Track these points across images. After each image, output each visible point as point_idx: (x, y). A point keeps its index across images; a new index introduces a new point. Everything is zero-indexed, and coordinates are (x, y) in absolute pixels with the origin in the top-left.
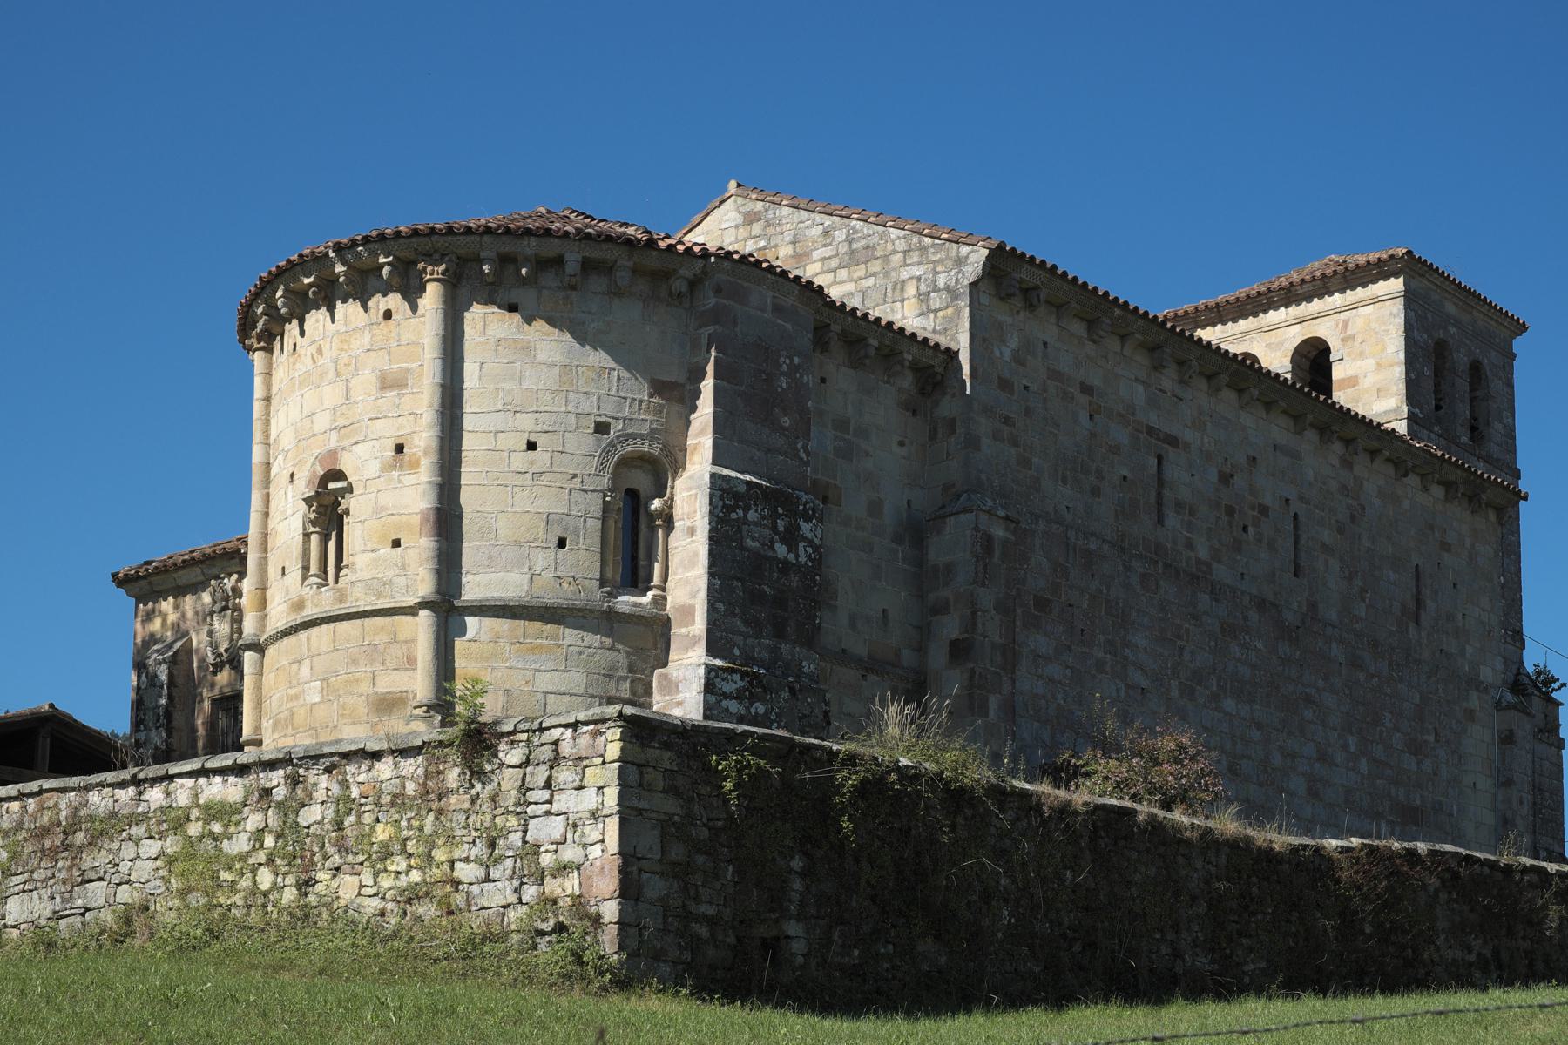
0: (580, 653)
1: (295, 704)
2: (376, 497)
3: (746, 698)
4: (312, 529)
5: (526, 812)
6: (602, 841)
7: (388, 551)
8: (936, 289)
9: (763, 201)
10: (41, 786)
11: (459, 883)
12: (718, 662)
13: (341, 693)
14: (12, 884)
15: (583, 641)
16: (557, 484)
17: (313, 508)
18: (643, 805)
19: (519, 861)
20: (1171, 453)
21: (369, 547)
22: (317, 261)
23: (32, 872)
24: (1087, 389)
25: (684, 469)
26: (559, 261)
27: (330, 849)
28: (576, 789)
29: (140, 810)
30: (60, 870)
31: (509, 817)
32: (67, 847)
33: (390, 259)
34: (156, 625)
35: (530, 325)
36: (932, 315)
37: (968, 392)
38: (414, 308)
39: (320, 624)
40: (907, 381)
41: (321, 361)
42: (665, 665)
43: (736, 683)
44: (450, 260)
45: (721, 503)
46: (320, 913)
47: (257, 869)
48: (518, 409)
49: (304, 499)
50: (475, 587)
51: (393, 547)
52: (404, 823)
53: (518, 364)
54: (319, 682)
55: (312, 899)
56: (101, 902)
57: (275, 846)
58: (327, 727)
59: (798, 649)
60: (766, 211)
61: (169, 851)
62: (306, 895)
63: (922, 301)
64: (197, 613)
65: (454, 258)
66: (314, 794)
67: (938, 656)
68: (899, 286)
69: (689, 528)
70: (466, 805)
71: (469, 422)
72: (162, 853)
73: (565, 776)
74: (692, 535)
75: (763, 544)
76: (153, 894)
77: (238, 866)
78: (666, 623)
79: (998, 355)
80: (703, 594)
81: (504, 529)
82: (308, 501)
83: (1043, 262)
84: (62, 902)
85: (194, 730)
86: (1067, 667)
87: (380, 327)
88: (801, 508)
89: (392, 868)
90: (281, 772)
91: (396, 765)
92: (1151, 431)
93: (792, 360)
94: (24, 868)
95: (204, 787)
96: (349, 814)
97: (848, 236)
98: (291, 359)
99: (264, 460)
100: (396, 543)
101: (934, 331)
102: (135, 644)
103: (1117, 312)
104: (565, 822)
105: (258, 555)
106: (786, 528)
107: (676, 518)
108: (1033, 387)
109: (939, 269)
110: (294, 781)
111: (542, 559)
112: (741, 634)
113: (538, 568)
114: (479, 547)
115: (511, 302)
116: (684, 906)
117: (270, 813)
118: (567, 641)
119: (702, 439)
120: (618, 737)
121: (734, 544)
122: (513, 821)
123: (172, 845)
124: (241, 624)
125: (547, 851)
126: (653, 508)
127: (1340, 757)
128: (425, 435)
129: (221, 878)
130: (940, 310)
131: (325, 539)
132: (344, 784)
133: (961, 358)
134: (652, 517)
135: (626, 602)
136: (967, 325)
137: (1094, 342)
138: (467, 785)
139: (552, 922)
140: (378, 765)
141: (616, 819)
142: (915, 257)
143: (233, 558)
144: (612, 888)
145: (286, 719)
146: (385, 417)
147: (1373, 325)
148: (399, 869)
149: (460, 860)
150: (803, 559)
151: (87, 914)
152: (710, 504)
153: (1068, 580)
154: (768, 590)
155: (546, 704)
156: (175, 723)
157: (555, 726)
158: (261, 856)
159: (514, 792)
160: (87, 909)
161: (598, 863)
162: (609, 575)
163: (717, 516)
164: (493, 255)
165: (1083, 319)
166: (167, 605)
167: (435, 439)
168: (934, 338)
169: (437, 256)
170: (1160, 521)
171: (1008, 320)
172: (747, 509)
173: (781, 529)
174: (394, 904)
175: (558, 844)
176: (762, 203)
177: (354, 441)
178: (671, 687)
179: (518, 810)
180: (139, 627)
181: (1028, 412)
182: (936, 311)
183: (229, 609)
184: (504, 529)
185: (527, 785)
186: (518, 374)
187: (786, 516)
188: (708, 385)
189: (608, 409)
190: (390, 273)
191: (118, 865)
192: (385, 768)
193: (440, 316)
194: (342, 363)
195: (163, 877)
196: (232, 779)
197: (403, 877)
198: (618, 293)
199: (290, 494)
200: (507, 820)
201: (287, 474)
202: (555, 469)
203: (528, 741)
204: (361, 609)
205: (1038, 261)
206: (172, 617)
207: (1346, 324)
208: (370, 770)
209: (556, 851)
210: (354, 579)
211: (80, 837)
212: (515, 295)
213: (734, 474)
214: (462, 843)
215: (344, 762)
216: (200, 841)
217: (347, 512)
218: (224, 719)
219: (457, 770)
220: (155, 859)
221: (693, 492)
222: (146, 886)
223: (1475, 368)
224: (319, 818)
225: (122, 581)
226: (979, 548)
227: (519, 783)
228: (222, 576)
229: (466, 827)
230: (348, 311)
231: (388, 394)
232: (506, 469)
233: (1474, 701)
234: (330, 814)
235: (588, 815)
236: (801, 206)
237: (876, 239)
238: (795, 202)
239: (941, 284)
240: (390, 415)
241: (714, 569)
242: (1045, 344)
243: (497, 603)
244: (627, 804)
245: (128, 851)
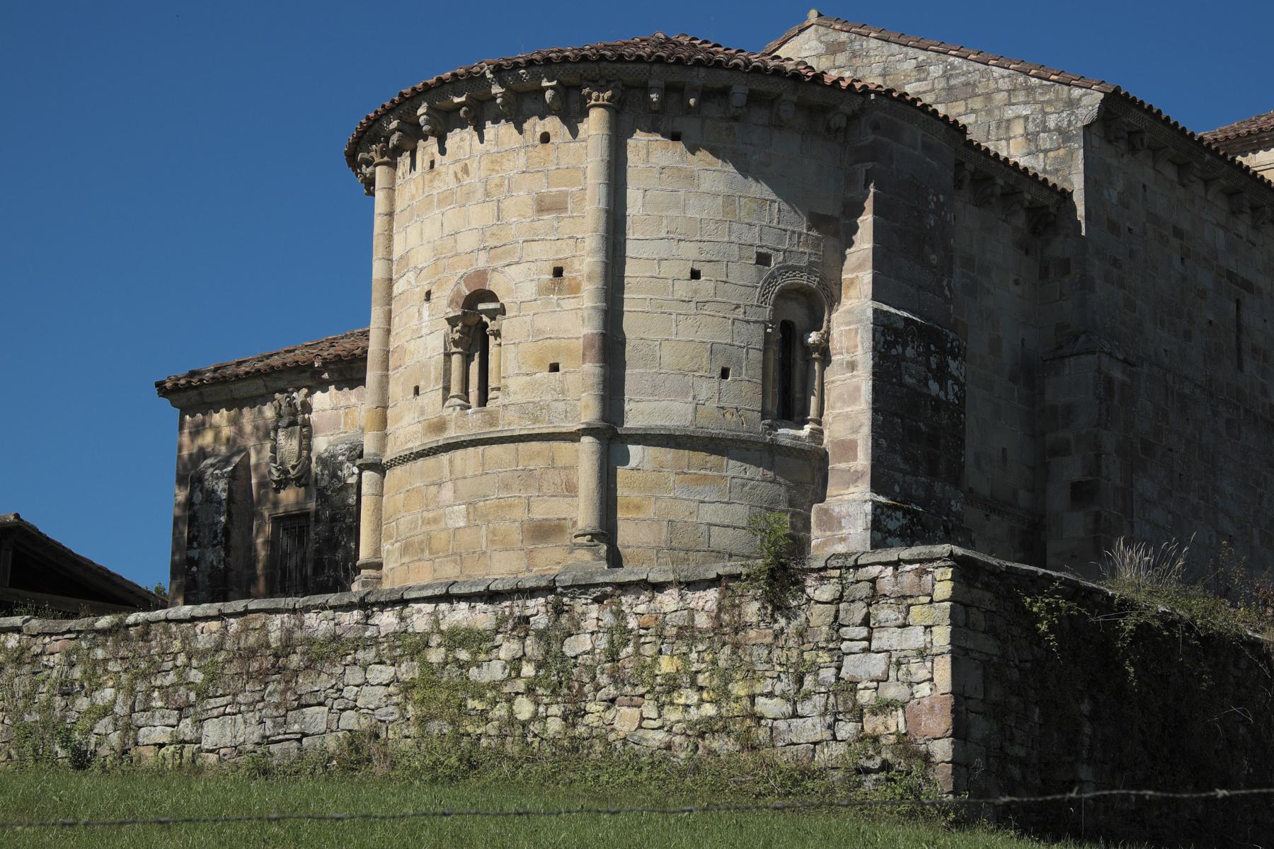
0: (743, 485)
1: (434, 527)
2: (532, 321)
3: (908, 536)
4: (454, 349)
5: (840, 649)
6: (931, 680)
7: (545, 374)
8: (1045, 129)
9: (848, 32)
10: (246, 606)
11: (762, 718)
12: (882, 499)
13: (491, 517)
14: (209, 707)
15: (746, 472)
16: (720, 314)
17: (458, 328)
18: (970, 645)
19: (832, 697)
21: (524, 370)
22: (473, 81)
23: (235, 695)
24: (1178, 233)
25: (839, 303)
26: (725, 93)
27: (603, 679)
28: (899, 627)
29: (368, 634)
30: (270, 694)
31: (821, 653)
32: (280, 670)
33: (554, 83)
34: (207, 439)
35: (694, 154)
36: (1041, 156)
37: (1083, 233)
38: (574, 133)
39: (466, 447)
40: (1021, 221)
41: (467, 181)
42: (822, 500)
43: (898, 520)
44: (616, 87)
45: (882, 339)
46: (591, 746)
47: (514, 698)
48: (682, 238)
49: (447, 319)
50: (637, 415)
51: (551, 371)
52: (694, 656)
53: (682, 193)
54: (464, 506)
55: (581, 730)
56: (323, 727)
57: (536, 676)
58: (474, 553)
59: (947, 487)
60: (851, 41)
61: (406, 677)
62: (574, 725)
63: (1030, 141)
64: (257, 428)
65: (620, 85)
66: (583, 624)
67: (532, 574)
68: (1004, 124)
69: (848, 363)
70: (769, 640)
71: (631, 249)
72: (395, 680)
73: (885, 613)
74: (853, 370)
75: (919, 381)
76: (384, 721)
77: (489, 695)
78: (824, 457)
79: (1107, 197)
80: (866, 430)
81: (668, 357)
82: (452, 321)
83: (1150, 107)
84: (274, 726)
85: (251, 548)
86: (1169, 512)
87: (536, 150)
88: (949, 345)
89: (682, 701)
90: (541, 600)
91: (682, 597)
92: (1231, 276)
93: (938, 199)
94: (225, 690)
95: (446, 613)
96: (626, 645)
97: (945, 72)
98: (428, 177)
99: (386, 276)
101: (1045, 171)
102: (179, 457)
103: (1208, 157)
105: (379, 372)
106: (938, 367)
107: (832, 352)
110: (558, 610)
111: (706, 389)
112: (901, 471)
113: (702, 397)
114: (642, 375)
115: (676, 130)
116: (1001, 748)
117: (528, 642)
118: (730, 473)
119: (861, 274)
120: (949, 576)
121: (894, 380)
122: (824, 658)
123: (408, 671)
124: (310, 440)
125: (866, 688)
126: (810, 340)
128: (589, 260)
129: (469, 706)
130: (1050, 150)
131: (467, 360)
132: (619, 614)
133: (1075, 199)
134: (808, 349)
135: (785, 434)
136: (1081, 167)
137: (1184, 186)
138: (768, 620)
139: (878, 760)
140: (660, 597)
141: (948, 658)
142: (1021, 96)
143: (304, 372)
144: (944, 727)
145: (421, 543)
146: (543, 240)
148: (689, 702)
149: (762, 695)
150: (951, 397)
151: (304, 740)
152: (873, 340)
153: (1168, 424)
155: (710, 536)
156: (233, 542)
157: (873, 564)
158: (520, 685)
159: (825, 629)
160: (305, 735)
161: (926, 702)
162: (769, 407)
163: (879, 352)
164: (662, 84)
165: (1174, 163)
166: (220, 418)
167: (600, 264)
168: (1052, 180)
169: (603, 82)
170: (1240, 367)
172: (905, 345)
173: (934, 366)
174: (683, 737)
175: (878, 681)
176: (846, 34)
177: (507, 262)
178: (831, 522)
179: (831, 646)
180: (186, 439)
182: (1046, 151)
183: (297, 424)
184: (668, 357)
185: (840, 620)
186: (682, 203)
187: (938, 353)
188: (866, 221)
189: (770, 241)
190: (554, 97)
191: (342, 690)
192: (668, 601)
193: (605, 143)
194: (492, 184)
195: (397, 704)
196: (480, 606)
197: (693, 710)
198: (779, 125)
199: (426, 313)
200: (818, 656)
201: (420, 292)
202: (719, 299)
203: (840, 577)
204: (516, 433)
205: (1146, 106)
206: (227, 431)
208: (650, 602)
209: (876, 689)
210: (506, 402)
211: (295, 660)
212: (679, 124)
213: (893, 310)
214: (765, 678)
215: (618, 592)
216: (443, 668)
217: (497, 334)
218: (285, 539)
219: (757, 605)
220: (388, 685)
221: (853, 327)
222: (376, 712)
224: (589, 647)
226: (1102, 390)
227: (832, 619)
228: (291, 390)
229: (769, 661)
230: (500, 133)
231: (545, 217)
232: (670, 297)
234: (603, 643)
235: (914, 653)
236: (892, 39)
237: (977, 76)
238: (884, 34)
239: (1052, 125)
240: (548, 238)
241: (878, 405)
242: (1144, 186)
243: (662, 432)
244: (957, 643)
245: (354, 676)
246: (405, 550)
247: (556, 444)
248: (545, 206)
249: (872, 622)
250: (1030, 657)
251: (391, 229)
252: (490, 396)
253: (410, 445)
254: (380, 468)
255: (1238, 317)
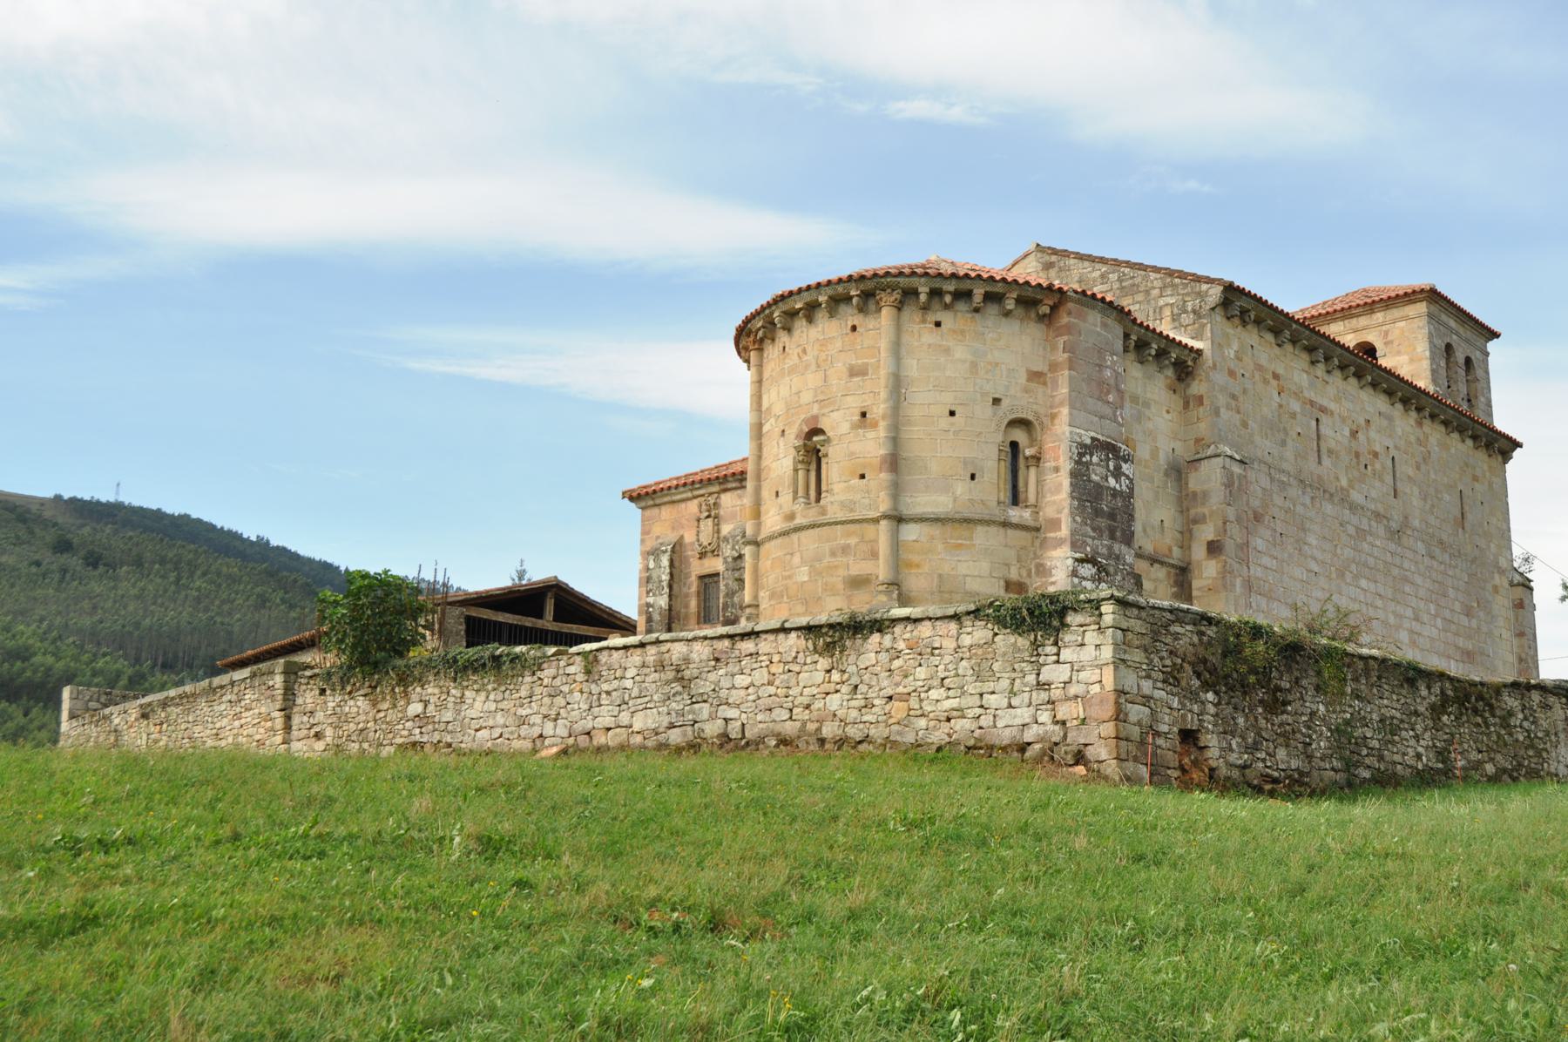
1: (788, 581)
6: (1101, 681)
7: (856, 481)
8: (1185, 312)
20: (1324, 419)
21: (843, 479)
24: (1276, 376)
52: (941, 667)
67: (1199, 552)
75: (1102, 478)
92: (1312, 403)
98: (781, 357)
100: (862, 477)
104: (1069, 669)
108: (1247, 375)
109: (1186, 299)
119: (1062, 409)
122: (1027, 667)
125: (1057, 688)
127: (1425, 618)
128: (882, 406)
147: (1406, 334)
150: (1124, 488)
154: (1105, 508)
160: (696, 722)
171: (1232, 332)
173: (1112, 468)
175: (1065, 683)
181: (1245, 391)
198: (1007, 314)
199: (781, 444)
201: (778, 430)
207: (1386, 333)
217: (826, 455)
220: (747, 688)
221: (1057, 444)
223: (1468, 361)
225: (635, 497)
233: (1497, 580)
237: (1139, 280)
246: (772, 596)
247: (865, 525)
248: (855, 372)
249: (1060, 643)
250: (1170, 664)
251: (760, 391)
252: (823, 496)
253: (774, 529)
254: (757, 544)
255: (1318, 430)
